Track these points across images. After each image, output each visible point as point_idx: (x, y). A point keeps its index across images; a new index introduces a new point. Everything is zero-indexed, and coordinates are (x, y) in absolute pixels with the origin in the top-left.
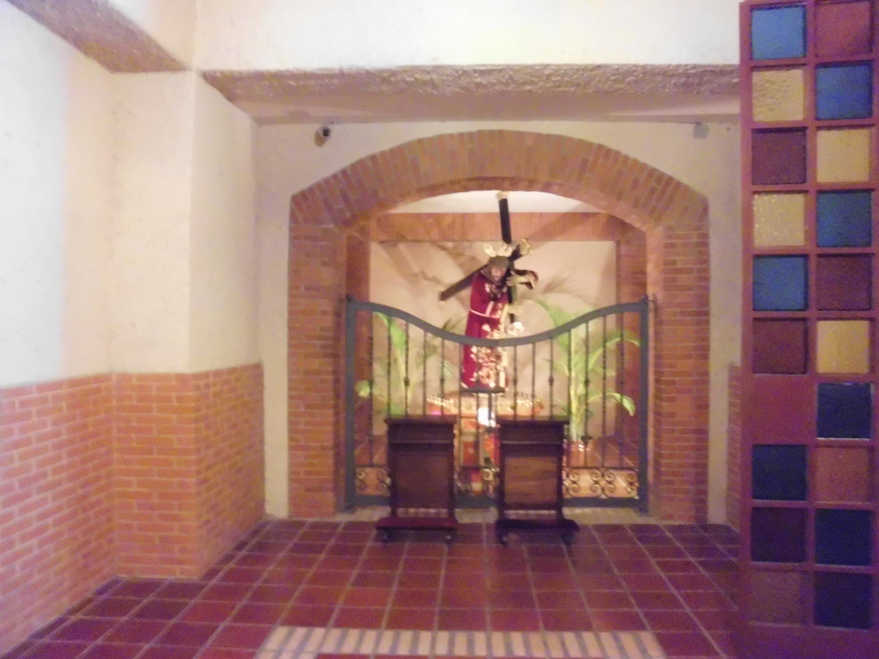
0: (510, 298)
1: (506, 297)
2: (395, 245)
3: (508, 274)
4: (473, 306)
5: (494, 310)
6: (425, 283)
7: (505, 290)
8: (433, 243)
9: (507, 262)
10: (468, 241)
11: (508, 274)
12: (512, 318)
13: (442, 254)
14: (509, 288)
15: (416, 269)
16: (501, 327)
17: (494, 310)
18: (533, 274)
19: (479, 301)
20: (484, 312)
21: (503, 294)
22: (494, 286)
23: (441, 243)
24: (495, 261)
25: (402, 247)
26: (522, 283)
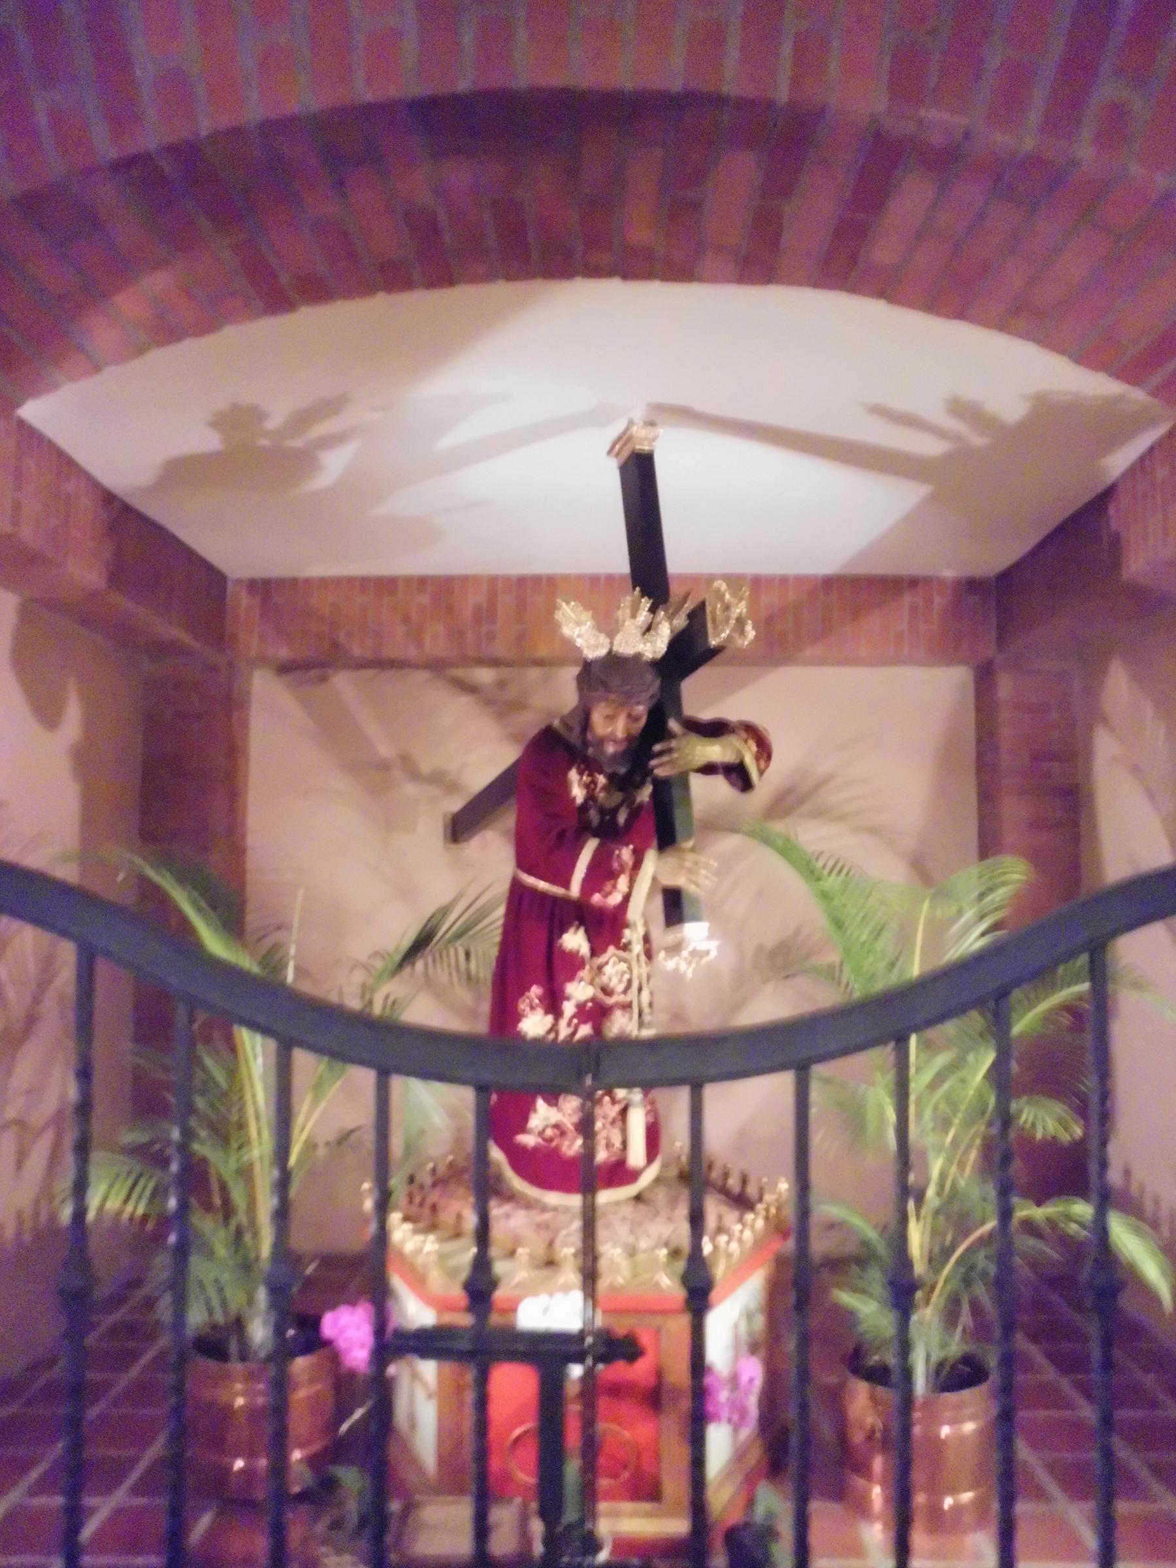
0: (664, 826)
1: (648, 823)
2: (323, 679)
3: (655, 730)
4: (524, 861)
5: (601, 873)
6: (411, 789)
7: (645, 794)
8: (436, 666)
9: (653, 684)
10: (539, 663)
11: (655, 730)
12: (675, 906)
13: (463, 703)
14: (662, 788)
15: (385, 750)
16: (633, 935)
17: (601, 873)
18: (752, 731)
19: (547, 835)
20: (566, 884)
21: (636, 813)
22: (602, 780)
23: (460, 672)
24: (602, 676)
25: (343, 682)
26: (709, 769)
